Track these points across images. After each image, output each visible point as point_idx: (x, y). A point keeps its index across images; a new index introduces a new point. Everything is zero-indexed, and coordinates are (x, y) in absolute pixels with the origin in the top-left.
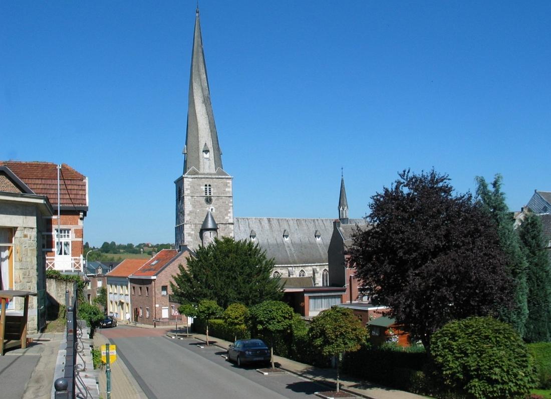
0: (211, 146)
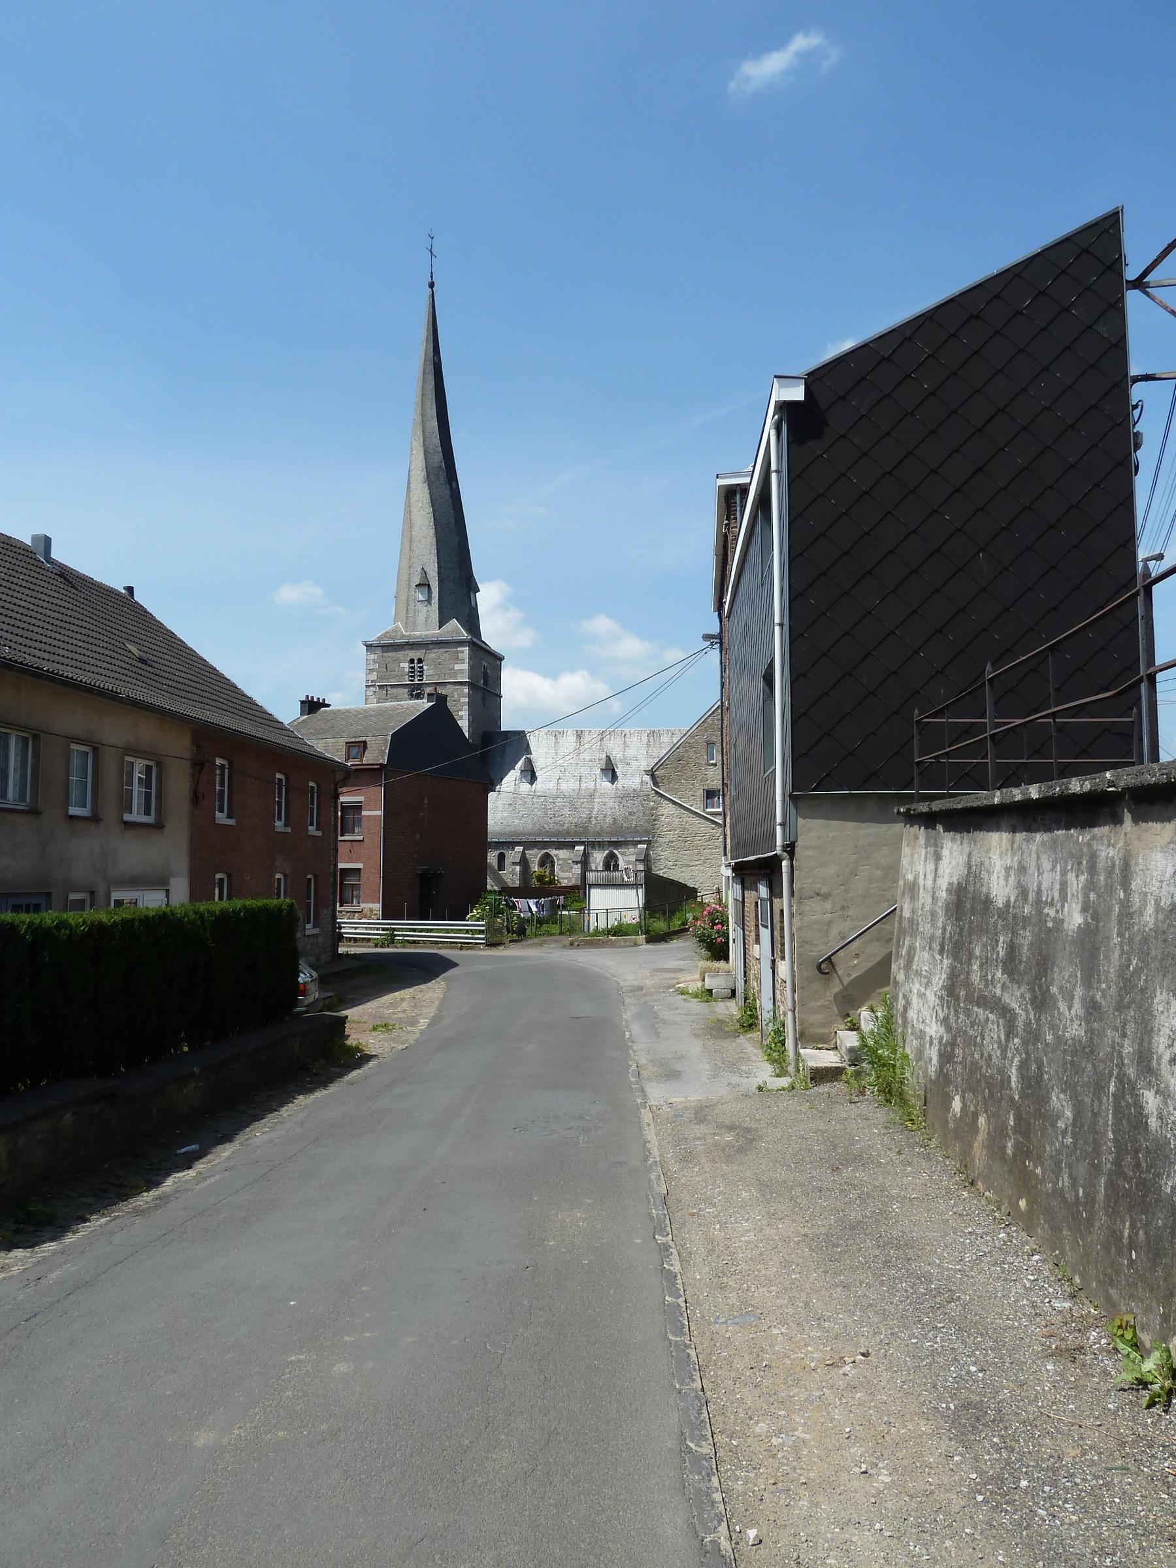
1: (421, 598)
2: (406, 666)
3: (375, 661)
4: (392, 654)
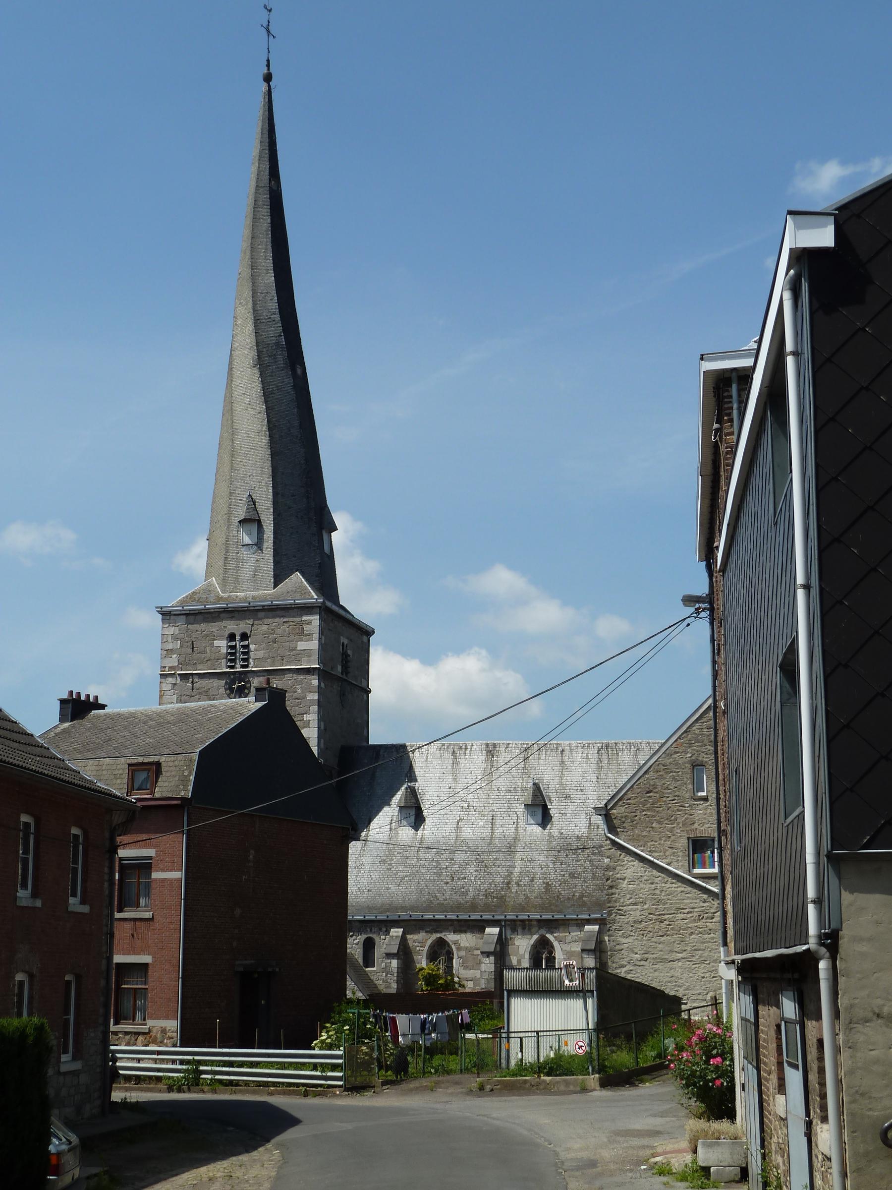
0: (270, 504)
1: (247, 540)
2: (222, 644)
3: (175, 638)
4: (202, 626)
